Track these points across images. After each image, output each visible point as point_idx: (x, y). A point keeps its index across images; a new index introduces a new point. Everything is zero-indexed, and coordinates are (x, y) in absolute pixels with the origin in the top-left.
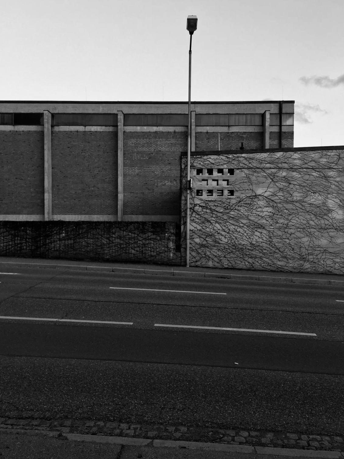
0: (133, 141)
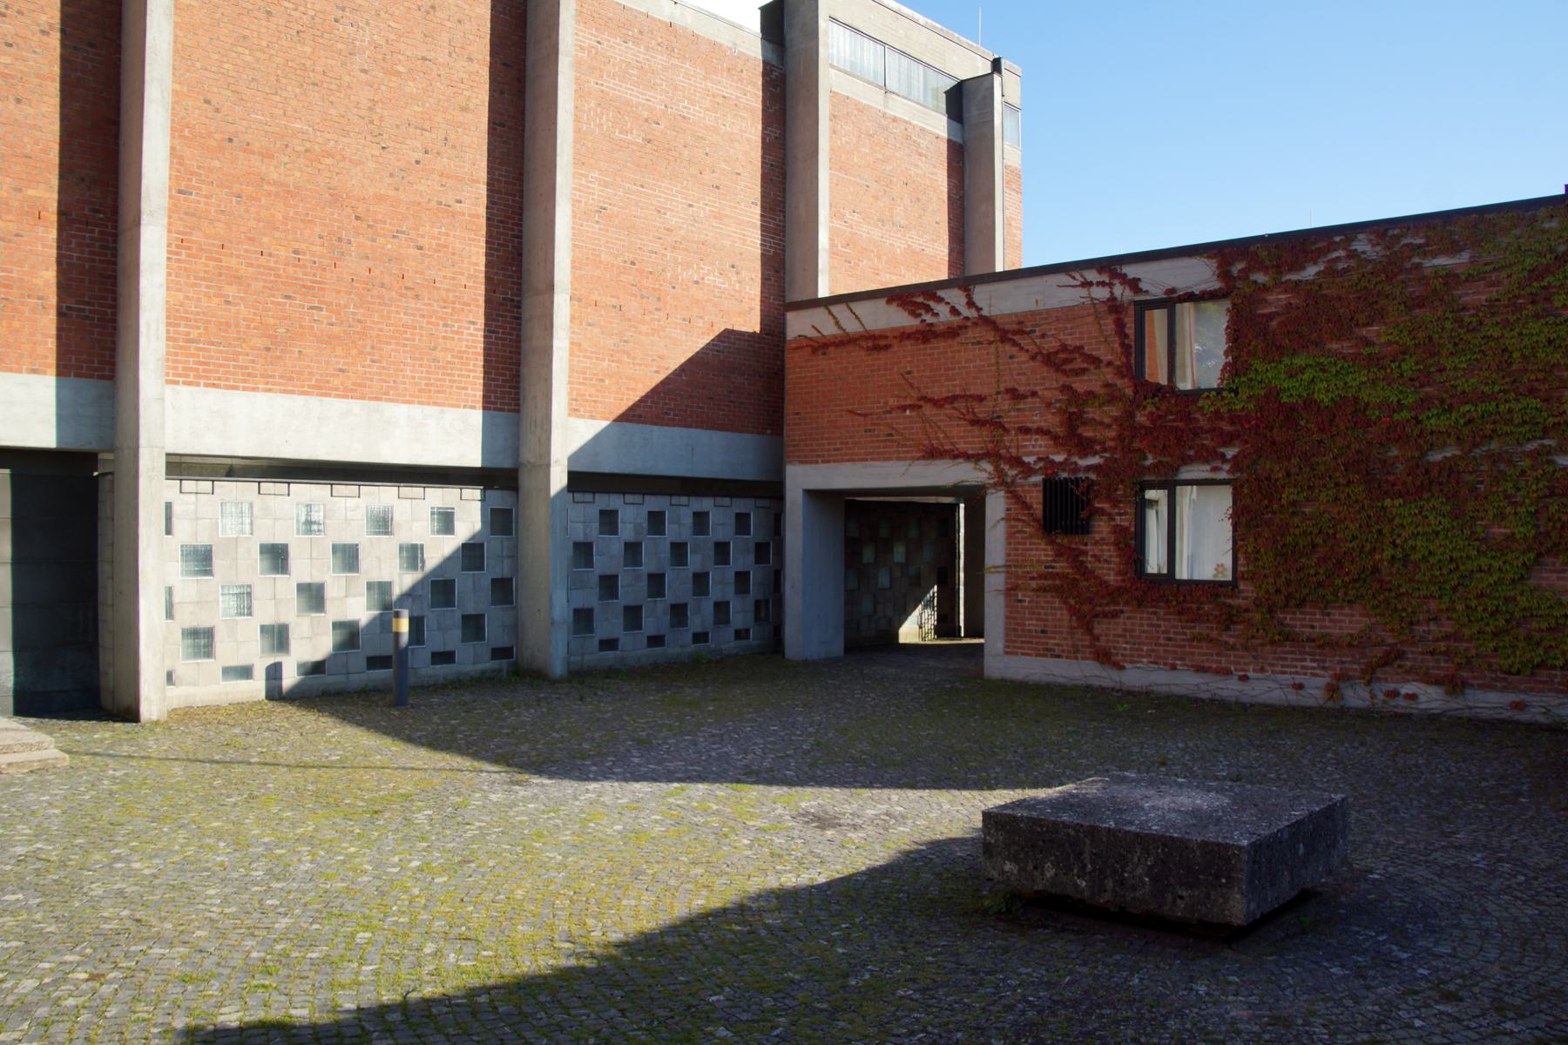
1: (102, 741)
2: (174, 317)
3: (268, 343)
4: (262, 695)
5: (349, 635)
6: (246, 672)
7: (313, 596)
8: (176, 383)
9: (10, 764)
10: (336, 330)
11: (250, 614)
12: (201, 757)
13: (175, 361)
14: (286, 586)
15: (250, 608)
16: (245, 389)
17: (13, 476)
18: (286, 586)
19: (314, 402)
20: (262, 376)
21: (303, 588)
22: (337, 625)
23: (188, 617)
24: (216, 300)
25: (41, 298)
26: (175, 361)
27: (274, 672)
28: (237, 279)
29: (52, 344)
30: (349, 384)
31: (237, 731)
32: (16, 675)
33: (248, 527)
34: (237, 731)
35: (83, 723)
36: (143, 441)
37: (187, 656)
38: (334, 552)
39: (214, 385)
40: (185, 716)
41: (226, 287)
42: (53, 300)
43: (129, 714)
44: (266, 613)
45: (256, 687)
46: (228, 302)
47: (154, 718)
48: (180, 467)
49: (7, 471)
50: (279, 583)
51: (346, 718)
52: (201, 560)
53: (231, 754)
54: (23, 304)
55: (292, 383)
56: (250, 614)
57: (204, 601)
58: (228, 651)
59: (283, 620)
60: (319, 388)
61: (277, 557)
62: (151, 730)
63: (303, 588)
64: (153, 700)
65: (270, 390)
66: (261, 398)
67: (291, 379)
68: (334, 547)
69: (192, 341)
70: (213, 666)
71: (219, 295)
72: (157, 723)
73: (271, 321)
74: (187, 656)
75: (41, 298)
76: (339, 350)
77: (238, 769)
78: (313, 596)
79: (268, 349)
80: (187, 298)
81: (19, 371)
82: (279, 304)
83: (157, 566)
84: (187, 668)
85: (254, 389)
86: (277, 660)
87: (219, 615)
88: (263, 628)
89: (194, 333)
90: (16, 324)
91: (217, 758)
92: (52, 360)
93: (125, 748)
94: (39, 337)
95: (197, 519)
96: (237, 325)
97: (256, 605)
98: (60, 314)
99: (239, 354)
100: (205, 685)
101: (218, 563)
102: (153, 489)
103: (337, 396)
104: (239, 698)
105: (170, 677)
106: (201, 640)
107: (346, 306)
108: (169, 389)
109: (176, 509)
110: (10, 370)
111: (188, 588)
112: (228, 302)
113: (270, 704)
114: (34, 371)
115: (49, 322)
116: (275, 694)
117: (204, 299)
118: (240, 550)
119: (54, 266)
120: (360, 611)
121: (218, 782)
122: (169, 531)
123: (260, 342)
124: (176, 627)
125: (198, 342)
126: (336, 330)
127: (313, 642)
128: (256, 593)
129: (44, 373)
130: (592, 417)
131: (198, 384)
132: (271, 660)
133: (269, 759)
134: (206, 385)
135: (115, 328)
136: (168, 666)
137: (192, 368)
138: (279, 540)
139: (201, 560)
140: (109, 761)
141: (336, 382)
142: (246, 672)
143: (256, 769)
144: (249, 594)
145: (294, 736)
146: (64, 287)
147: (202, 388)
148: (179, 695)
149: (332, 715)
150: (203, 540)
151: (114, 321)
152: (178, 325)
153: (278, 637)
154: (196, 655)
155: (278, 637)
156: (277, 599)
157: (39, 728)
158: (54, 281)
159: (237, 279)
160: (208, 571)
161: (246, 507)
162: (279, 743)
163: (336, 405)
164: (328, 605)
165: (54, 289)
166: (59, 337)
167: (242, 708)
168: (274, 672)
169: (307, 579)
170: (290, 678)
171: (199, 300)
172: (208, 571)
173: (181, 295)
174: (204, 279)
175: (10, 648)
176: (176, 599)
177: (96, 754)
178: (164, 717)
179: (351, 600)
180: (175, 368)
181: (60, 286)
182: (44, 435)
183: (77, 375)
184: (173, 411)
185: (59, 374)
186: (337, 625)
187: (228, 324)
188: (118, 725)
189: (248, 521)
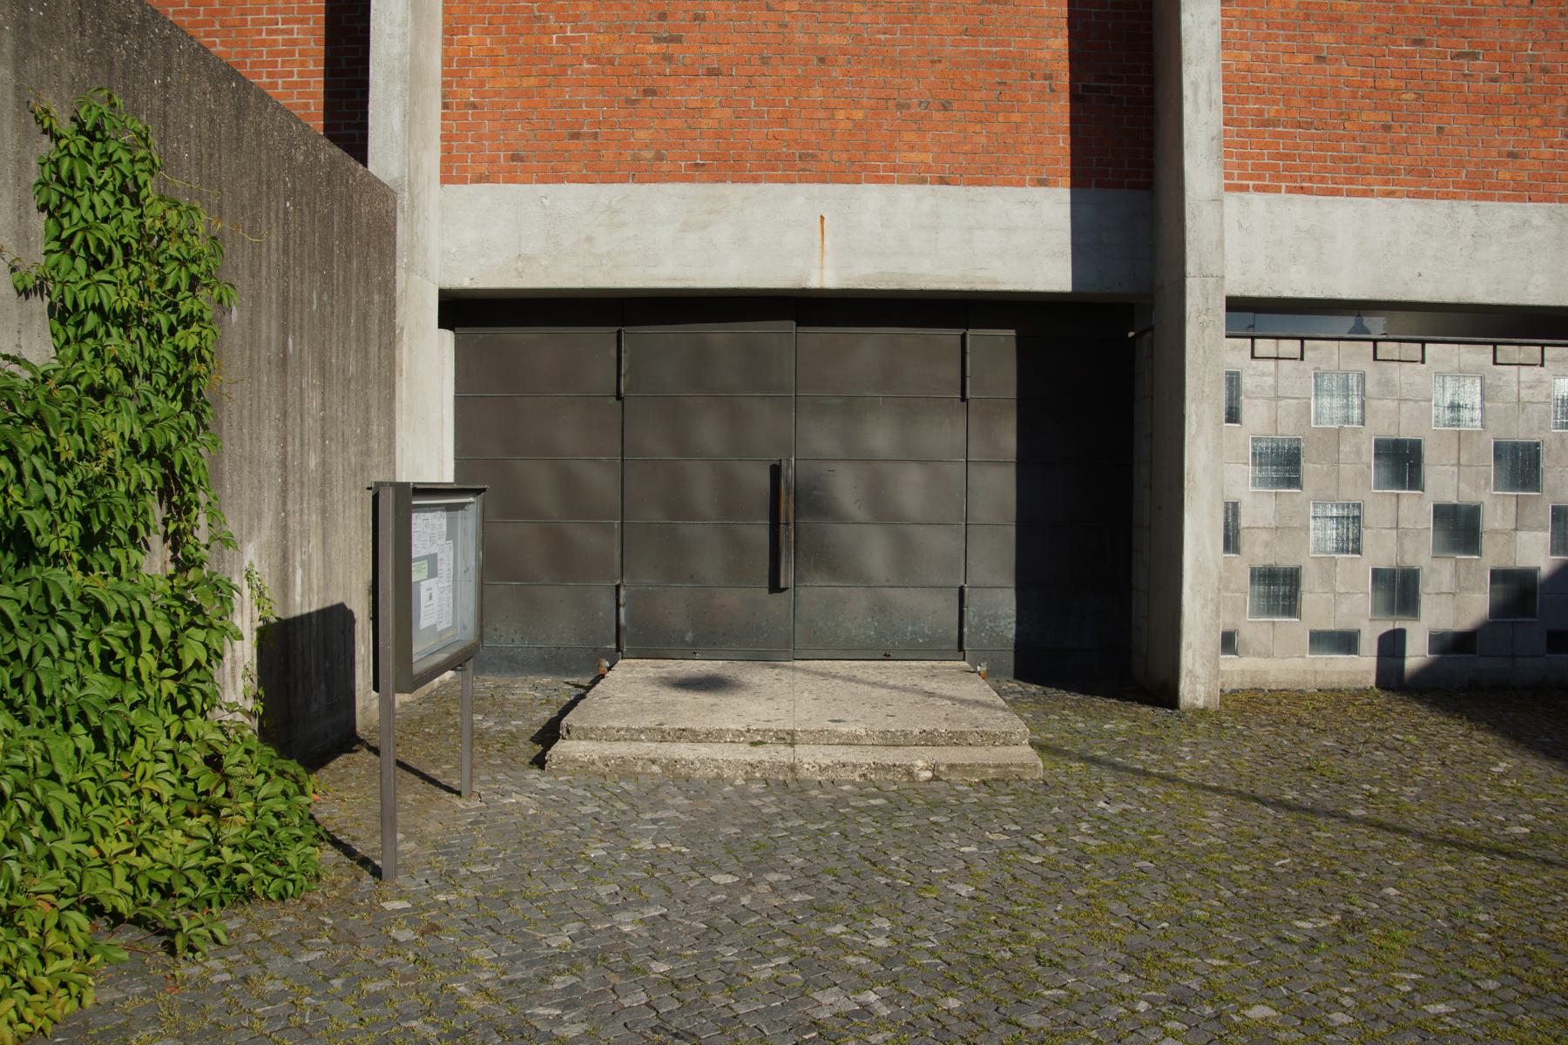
1: (1112, 735)
2: (1234, 88)
3: (1387, 118)
4: (1371, 680)
5: (1516, 589)
6: (1346, 642)
7: (1460, 527)
8: (1245, 189)
9: (951, 767)
10: (1503, 88)
11: (1357, 551)
12: (1260, 791)
13: (1241, 156)
14: (1417, 509)
15: (1357, 540)
16: (1350, 194)
17: (1019, 340)
18: (1417, 509)
19: (1465, 210)
20: (1378, 171)
21: (1444, 514)
22: (1498, 576)
23: (1259, 551)
24: (1302, 57)
25: (1048, 77)
26: (1241, 156)
27: (1392, 645)
29: (1063, 142)
30: (1524, 176)
31: (1328, 742)
32: (1018, 623)
33: (1356, 413)
34: (1328, 742)
35: (1098, 701)
36: (1190, 268)
37: (1256, 612)
38: (1497, 457)
39: (1302, 190)
40: (1248, 704)
41: (1317, 36)
42: (1065, 79)
43: (1164, 693)
44: (1381, 551)
45: (1362, 666)
46: (1320, 59)
47: (1200, 703)
48: (1252, 314)
49: (1012, 332)
50: (1404, 503)
51: (1520, 736)
52: (1283, 464)
53: (1315, 793)
54: (1024, 89)
55: (1424, 181)
56: (1357, 551)
57: (1294, 528)
58: (1320, 606)
59: (1409, 561)
60: (1473, 186)
61: (1401, 461)
62: (1192, 725)
63: (1444, 514)
64: (1200, 675)
65: (1390, 194)
66: (1376, 206)
67: (1425, 174)
68: (1497, 446)
69: (1266, 123)
70: (1296, 629)
71: (1305, 50)
72: (1202, 713)
73: (1392, 83)
74: (1256, 612)
75: (1048, 77)
76: (1507, 122)
77: (1325, 832)
78: (1460, 527)
79: (1387, 128)
80: (1258, 58)
81: (1021, 184)
82: (1402, 55)
83: (1214, 469)
84: (1253, 628)
85: (1364, 194)
86: (1398, 625)
87: (1311, 544)
88: (1376, 572)
89: (1270, 111)
90: (1016, 117)
91: (1290, 795)
92: (1065, 165)
93: (1143, 755)
94: (1047, 133)
95: (1278, 398)
96: (1336, 95)
97: (1367, 536)
98: (1074, 98)
99: (1342, 138)
100: (1281, 658)
101: (1308, 468)
102: (1208, 351)
103: (1505, 198)
104: (1334, 681)
105: (1228, 642)
106: (1280, 588)
107: (1518, 47)
108: (1232, 200)
109: (1247, 383)
110: (1010, 184)
111: (1260, 506)
112: (1320, 59)
113: (1383, 697)
114: (1041, 183)
115: (1060, 110)
116: (1391, 675)
117: (1284, 58)
118: (1345, 448)
119: (1066, 32)
120: (1535, 552)
121: (1283, 862)
122: (1233, 416)
123: (1372, 118)
124: (1241, 566)
125: (1275, 123)
126: (1503, 88)
127: (1455, 601)
128: (1369, 516)
129: (1055, 184)
131: (1277, 190)
132: (1387, 626)
133: (1385, 816)
134: (1290, 190)
135: (1152, 112)
136: (1227, 622)
137: (1264, 165)
138: (1406, 434)
139: (1283, 464)
140: (1108, 778)
141: (1504, 175)
142: (1346, 642)
143: (1362, 836)
144: (1357, 519)
145: (1429, 765)
146: (1078, 58)
147: (1284, 195)
148: (1239, 670)
149: (1493, 728)
150: (1287, 430)
151: (1151, 101)
152: (1246, 101)
153: (1399, 589)
154: (1271, 610)
155: (1399, 589)
156: (1401, 529)
157: (1014, 705)
158: (1065, 51)
160: (1294, 481)
161: (1353, 381)
162: (1403, 778)
163: (1504, 213)
164: (1485, 542)
165: (1065, 64)
166: (1074, 131)
167: (1338, 698)
168: (1392, 645)
169: (1451, 498)
170: (1416, 654)
171: (1276, 59)
172: (1294, 481)
173: (1247, 55)
174: (1283, 27)
175: (1011, 582)
176: (1244, 522)
177: (1094, 760)
178: (1215, 705)
179: (1523, 536)
180: (1241, 166)
181: (1074, 57)
182: (1050, 271)
183: (1098, 185)
184: (1239, 233)
185: (1074, 185)
186: (1498, 576)
187: (1322, 95)
188: (1145, 709)
189: (1356, 401)
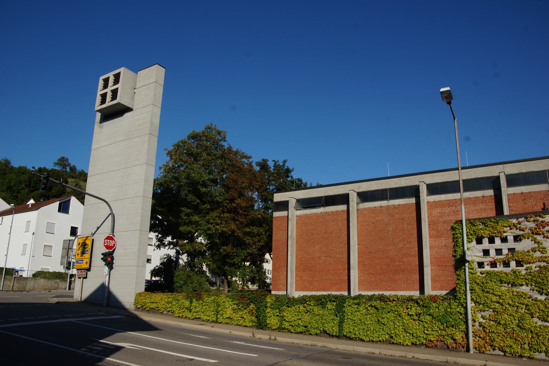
0: (438, 210)
28: (372, 274)
130: (442, 290)
159: (372, 274)
